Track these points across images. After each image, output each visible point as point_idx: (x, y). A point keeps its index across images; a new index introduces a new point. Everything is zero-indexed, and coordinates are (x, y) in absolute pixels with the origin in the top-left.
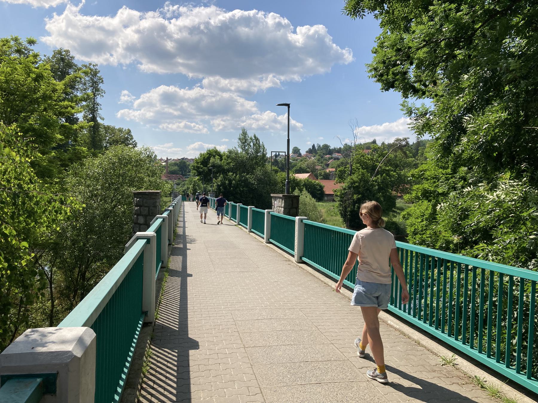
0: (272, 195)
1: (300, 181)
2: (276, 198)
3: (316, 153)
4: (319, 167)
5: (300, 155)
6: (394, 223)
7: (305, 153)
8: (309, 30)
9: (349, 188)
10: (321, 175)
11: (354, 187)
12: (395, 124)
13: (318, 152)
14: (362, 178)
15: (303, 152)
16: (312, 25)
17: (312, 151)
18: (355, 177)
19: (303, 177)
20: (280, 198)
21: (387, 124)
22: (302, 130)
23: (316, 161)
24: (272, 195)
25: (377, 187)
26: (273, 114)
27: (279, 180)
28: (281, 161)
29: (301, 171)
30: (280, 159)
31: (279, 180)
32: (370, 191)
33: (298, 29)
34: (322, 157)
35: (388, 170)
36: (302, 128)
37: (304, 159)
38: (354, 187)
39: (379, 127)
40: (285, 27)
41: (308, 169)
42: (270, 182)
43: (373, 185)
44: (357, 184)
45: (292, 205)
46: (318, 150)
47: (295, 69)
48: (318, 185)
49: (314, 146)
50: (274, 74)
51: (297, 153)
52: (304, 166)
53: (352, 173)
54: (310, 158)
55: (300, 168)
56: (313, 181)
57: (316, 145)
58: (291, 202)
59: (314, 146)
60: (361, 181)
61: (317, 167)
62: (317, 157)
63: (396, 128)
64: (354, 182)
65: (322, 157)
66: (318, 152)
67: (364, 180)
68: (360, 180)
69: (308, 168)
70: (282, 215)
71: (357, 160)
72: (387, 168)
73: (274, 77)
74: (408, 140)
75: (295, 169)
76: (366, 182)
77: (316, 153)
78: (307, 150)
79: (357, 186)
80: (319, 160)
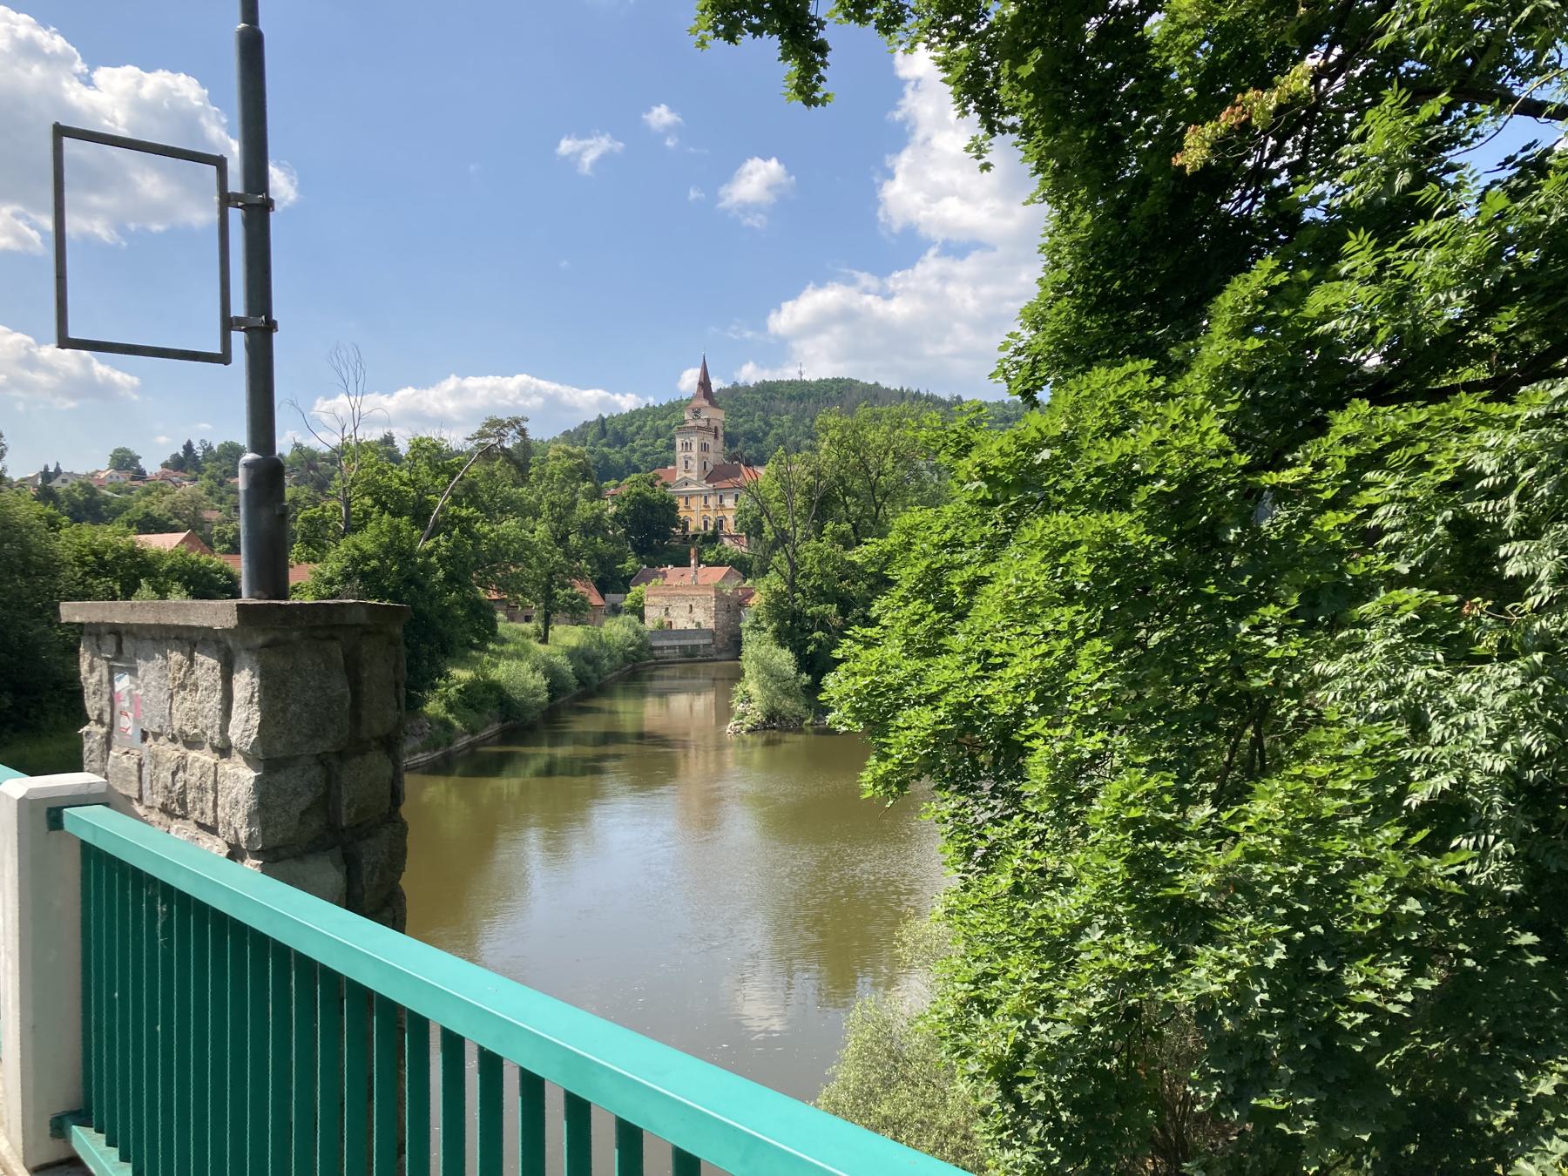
0: (72, 612)
1: (160, 556)
2: (124, 644)
3: (200, 470)
4: (214, 516)
5: (140, 475)
6: (494, 687)
7: (159, 469)
8: (139, 84)
9: (347, 577)
10: (222, 540)
11: (364, 576)
12: (432, 393)
13: (207, 465)
14: (392, 543)
15: (152, 465)
16: (149, 68)
17: (185, 462)
18: (366, 540)
19: (163, 543)
20: (191, 640)
21: (411, 390)
22: (135, 397)
23: (202, 493)
24: (72, 612)
25: (441, 574)
26: (19, 336)
27: (68, 555)
28: (68, 494)
29: (159, 526)
30: (66, 486)
31: (68, 555)
32: (420, 587)
33: (102, 75)
34: (221, 484)
35: (468, 519)
36: (136, 390)
37: (155, 488)
38: (364, 576)
39: (383, 398)
40: (51, 59)
41: (175, 522)
42: (27, 562)
43: (427, 569)
44: (374, 563)
45: (356, 718)
46: (205, 459)
47: (95, 200)
48: (220, 570)
49: (188, 448)
50: (17, 208)
51: (127, 468)
52: (159, 509)
53: (353, 527)
54: (177, 485)
55: (147, 515)
56: (203, 559)
57: (196, 445)
58: (339, 687)
59: (188, 448)
60: (387, 553)
61: (207, 515)
62: (204, 481)
63: (437, 406)
64: (365, 558)
65: (221, 484)
66: (207, 465)
67: (397, 551)
68: (388, 550)
69: (177, 516)
70: (208, 863)
71: (367, 483)
72: (464, 513)
73: (17, 216)
74: (524, 425)
75: (125, 517)
76: (405, 556)
77: (200, 470)
78: (167, 457)
79: (375, 570)
80: (210, 493)
